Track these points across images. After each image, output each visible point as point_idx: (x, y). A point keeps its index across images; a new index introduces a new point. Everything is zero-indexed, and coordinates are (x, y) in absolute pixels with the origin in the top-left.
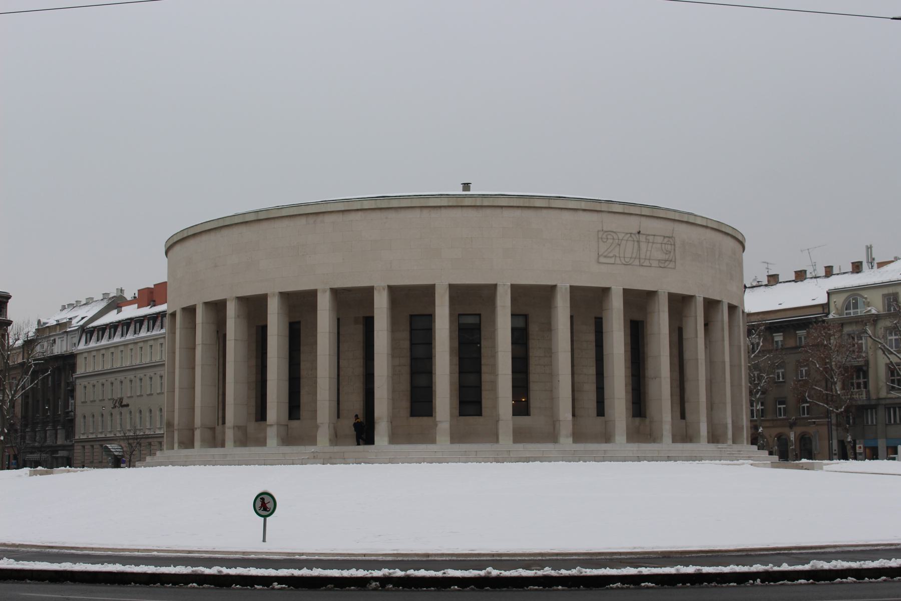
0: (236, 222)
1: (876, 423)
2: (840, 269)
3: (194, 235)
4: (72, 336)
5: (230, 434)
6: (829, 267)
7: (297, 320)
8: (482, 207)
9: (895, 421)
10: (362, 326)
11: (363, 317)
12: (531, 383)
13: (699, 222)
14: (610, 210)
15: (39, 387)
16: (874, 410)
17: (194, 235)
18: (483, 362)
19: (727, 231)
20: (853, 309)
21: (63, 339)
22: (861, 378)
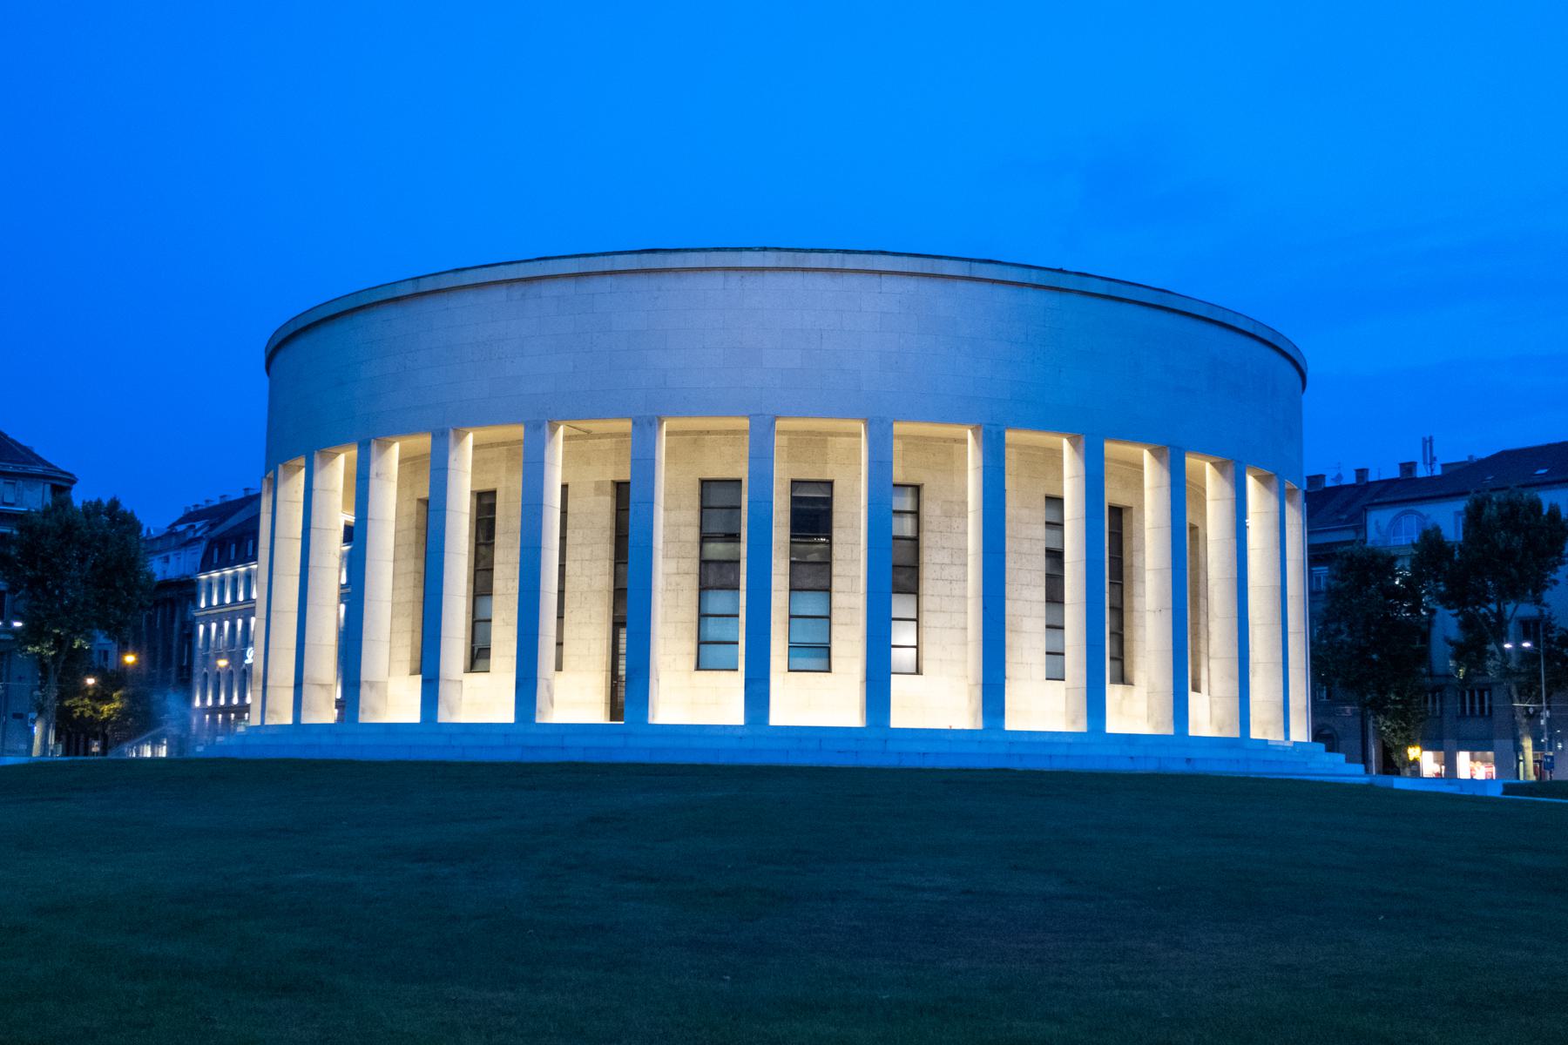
0: (379, 298)
2: (1379, 474)
5: (1515, 696)
7: (489, 487)
8: (842, 271)
9: (1472, 709)
11: (613, 482)
13: (1241, 325)
14: (1085, 289)
22: (1418, 642)
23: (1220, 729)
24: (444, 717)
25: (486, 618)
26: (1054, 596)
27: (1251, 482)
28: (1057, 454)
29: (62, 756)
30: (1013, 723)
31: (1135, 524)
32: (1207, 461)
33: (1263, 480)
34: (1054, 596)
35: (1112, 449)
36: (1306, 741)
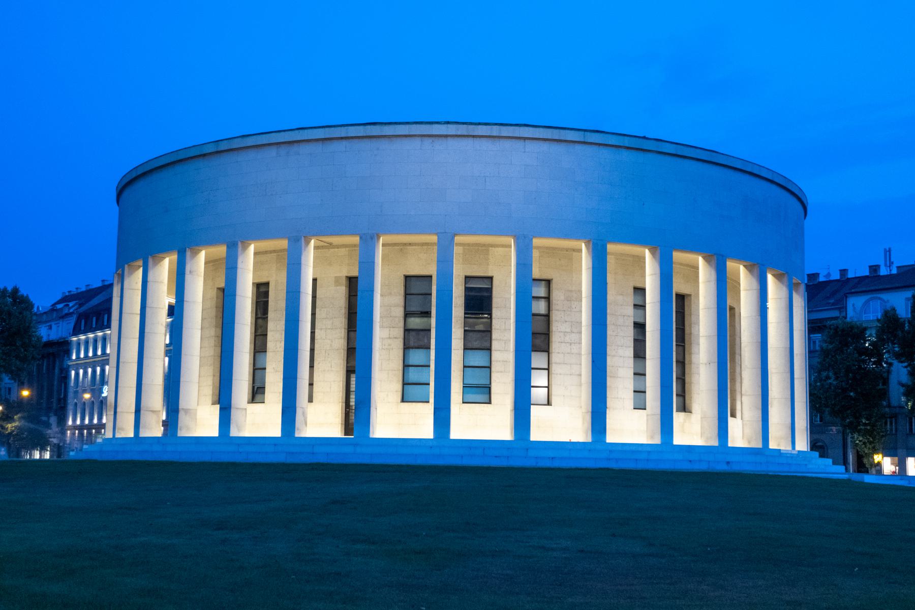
1: (896, 431)
2: (855, 273)
3: (144, 174)
4: (68, 322)
6: (844, 270)
10: (345, 288)
12: (553, 365)
14: (660, 150)
15: (34, 374)
16: (894, 420)
17: (144, 174)
18: (494, 336)
19: (793, 190)
20: (873, 313)
21: (58, 325)
24: (234, 432)
26: (639, 354)
27: (770, 278)
28: (641, 260)
30: (611, 438)
33: (779, 277)
34: (639, 354)
36: (806, 450)
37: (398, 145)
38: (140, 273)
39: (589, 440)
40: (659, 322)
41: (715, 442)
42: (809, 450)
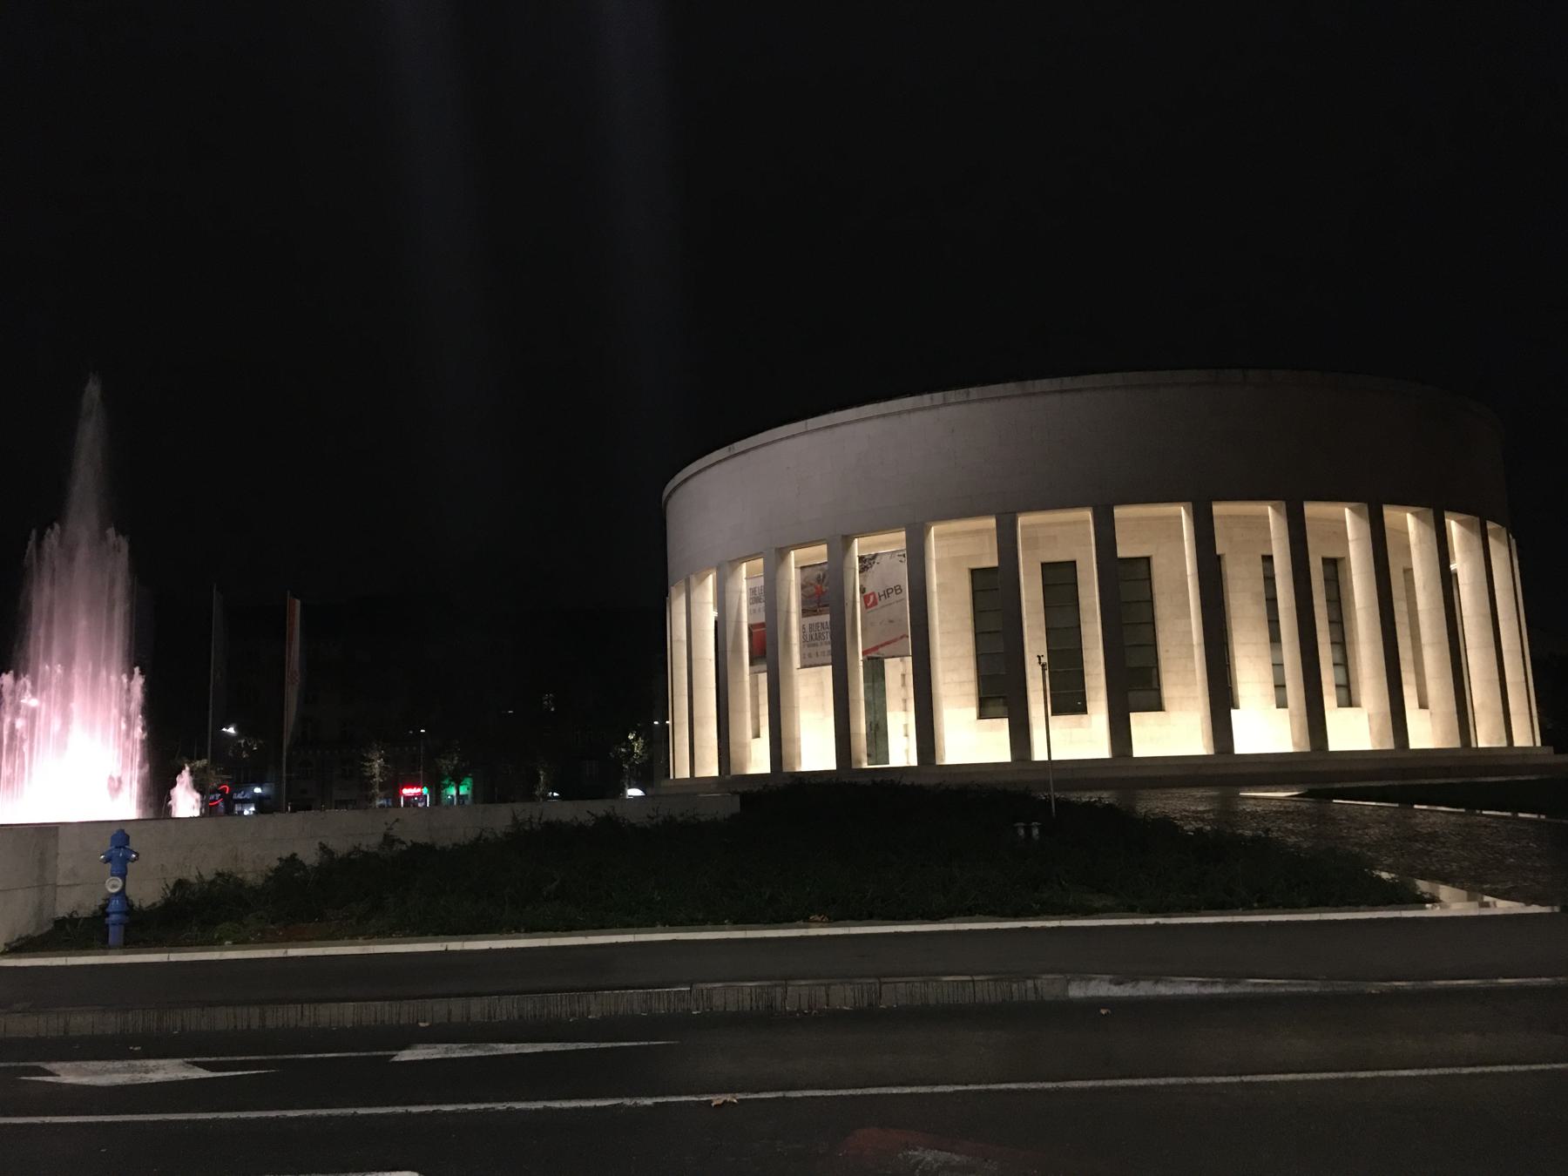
23: (1490, 742)
24: (698, 775)
25: (1337, 667)
27: (1454, 528)
29: (1057, 800)
30: (1334, 745)
31: (796, 728)
32: (1407, 512)
35: (1311, 509)
36: (1530, 744)
37: (692, 484)
38: (710, 581)
39: (1211, 752)
40: (1439, 580)
41: (1389, 744)
42: (1539, 744)
